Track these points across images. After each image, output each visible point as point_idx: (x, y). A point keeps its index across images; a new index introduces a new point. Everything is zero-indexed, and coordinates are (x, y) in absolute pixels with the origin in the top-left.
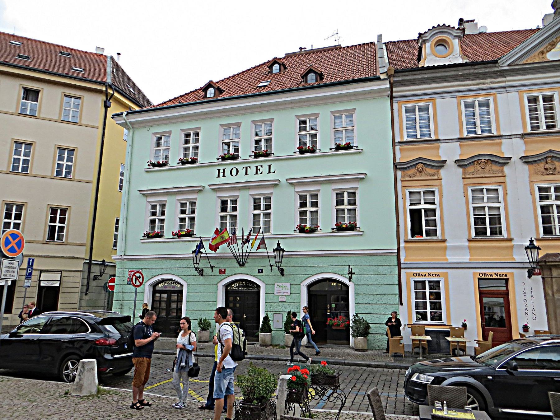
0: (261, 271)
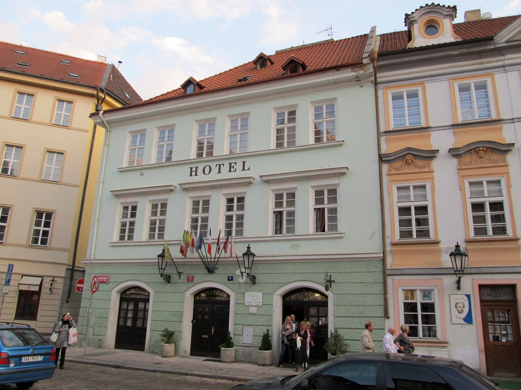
0: (230, 279)
